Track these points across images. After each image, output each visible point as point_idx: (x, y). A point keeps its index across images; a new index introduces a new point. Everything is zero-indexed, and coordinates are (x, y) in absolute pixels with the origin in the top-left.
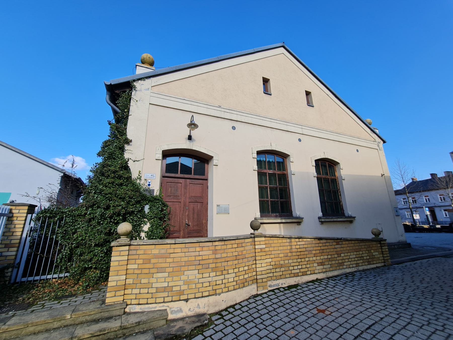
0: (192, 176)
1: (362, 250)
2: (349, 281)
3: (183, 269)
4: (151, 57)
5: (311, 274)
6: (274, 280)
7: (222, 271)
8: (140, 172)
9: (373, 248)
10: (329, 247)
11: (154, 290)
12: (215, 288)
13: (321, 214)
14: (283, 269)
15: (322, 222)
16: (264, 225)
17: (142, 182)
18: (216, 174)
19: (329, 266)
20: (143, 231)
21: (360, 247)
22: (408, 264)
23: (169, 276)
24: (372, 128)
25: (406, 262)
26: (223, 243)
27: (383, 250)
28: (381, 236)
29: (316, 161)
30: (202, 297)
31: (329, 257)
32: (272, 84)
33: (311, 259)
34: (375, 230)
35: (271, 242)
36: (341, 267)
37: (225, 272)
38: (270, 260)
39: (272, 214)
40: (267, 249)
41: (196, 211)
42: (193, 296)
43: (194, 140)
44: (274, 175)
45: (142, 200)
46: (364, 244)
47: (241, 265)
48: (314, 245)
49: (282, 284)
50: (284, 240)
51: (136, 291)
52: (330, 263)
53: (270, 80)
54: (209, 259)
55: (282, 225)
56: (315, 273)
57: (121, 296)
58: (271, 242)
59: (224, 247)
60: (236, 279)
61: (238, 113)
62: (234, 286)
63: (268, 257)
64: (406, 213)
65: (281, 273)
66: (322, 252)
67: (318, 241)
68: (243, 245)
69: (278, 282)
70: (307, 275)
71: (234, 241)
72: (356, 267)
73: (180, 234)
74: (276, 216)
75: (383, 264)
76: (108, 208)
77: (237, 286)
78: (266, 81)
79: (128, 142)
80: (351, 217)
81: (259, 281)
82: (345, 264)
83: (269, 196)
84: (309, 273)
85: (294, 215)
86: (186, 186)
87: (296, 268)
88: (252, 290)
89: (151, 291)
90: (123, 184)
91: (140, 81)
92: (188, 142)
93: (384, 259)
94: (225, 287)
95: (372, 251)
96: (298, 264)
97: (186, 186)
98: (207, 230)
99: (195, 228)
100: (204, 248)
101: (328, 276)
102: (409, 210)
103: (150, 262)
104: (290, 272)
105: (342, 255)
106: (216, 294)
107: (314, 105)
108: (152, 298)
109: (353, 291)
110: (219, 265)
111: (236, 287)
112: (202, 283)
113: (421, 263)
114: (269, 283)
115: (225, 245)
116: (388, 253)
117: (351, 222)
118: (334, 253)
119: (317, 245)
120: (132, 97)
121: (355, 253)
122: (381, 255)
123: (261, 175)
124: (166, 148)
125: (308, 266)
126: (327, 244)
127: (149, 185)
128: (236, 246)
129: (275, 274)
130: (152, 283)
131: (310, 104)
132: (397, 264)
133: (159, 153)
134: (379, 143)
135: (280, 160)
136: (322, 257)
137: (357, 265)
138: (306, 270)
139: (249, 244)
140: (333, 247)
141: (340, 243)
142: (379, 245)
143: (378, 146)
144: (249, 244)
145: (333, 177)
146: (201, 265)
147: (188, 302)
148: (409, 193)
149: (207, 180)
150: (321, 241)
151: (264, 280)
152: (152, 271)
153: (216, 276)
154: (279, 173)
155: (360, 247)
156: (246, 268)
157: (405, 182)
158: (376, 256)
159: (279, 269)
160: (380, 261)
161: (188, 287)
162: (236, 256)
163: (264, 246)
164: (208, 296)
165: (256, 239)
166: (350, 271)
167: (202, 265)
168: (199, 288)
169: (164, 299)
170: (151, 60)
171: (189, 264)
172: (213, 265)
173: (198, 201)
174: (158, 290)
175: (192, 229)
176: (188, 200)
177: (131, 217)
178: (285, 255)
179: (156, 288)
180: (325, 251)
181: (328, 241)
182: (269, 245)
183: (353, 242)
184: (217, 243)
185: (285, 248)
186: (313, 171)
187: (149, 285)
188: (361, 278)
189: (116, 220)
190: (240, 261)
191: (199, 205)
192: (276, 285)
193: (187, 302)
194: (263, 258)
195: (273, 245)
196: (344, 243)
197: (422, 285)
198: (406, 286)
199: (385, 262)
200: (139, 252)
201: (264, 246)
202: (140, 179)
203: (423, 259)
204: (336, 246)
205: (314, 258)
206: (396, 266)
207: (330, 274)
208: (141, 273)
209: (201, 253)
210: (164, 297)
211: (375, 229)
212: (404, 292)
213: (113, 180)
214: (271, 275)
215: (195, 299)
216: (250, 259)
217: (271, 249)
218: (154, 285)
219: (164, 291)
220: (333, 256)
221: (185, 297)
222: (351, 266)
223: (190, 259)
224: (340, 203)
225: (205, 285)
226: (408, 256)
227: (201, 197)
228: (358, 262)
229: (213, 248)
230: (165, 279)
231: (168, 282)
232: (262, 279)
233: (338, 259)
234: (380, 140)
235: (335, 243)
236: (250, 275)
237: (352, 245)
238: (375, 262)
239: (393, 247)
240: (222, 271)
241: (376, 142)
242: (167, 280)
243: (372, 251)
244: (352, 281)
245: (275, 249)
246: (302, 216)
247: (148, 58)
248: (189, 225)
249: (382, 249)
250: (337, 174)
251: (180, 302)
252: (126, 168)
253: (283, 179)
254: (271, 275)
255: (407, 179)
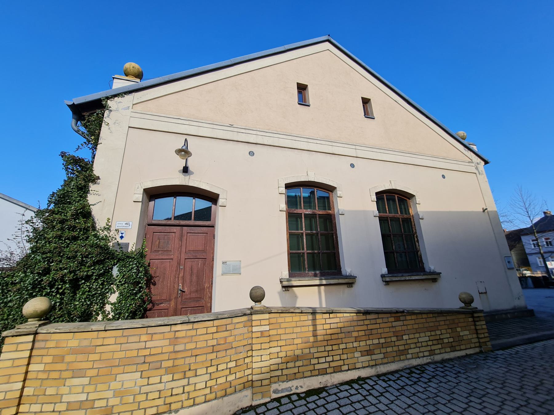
0: (192, 222)
1: (440, 328)
2: (410, 383)
3: (115, 370)
4: (137, 66)
5: (349, 370)
6: (283, 382)
7: (185, 372)
8: (109, 219)
9: (460, 325)
10: (382, 325)
12: (168, 400)
13: (385, 270)
14: (299, 363)
15: (386, 281)
16: (294, 289)
18: (226, 220)
19: (382, 356)
20: (108, 303)
21: (437, 324)
23: (89, 384)
25: (518, 345)
26: (190, 326)
27: (478, 327)
28: (473, 305)
29: (377, 194)
31: (382, 341)
32: (311, 91)
33: (350, 345)
34: (464, 296)
35: (280, 320)
36: (402, 357)
37: (189, 374)
38: (278, 349)
41: (195, 271)
43: (192, 173)
44: (313, 216)
45: (108, 258)
46: (444, 318)
48: (355, 323)
52: (383, 350)
53: (309, 86)
54: (162, 353)
55: (322, 287)
56: (355, 369)
58: (280, 320)
59: (193, 333)
62: (205, 395)
63: (275, 344)
64: (538, 260)
65: (296, 370)
66: (369, 334)
67: (362, 317)
68: (229, 327)
70: (341, 371)
71: (212, 322)
72: (430, 356)
73: (170, 304)
74: (315, 275)
75: (477, 350)
76: (47, 271)
77: (213, 396)
78: (302, 88)
79: (94, 179)
80: (434, 273)
81: (255, 384)
82: (410, 351)
83: (305, 246)
84: (346, 367)
85: (343, 273)
86: (182, 236)
87: (323, 360)
90: (79, 237)
91: (116, 98)
92: (181, 176)
93: (479, 342)
94: (189, 399)
95: (459, 329)
96: (326, 354)
97: (182, 236)
98: (211, 298)
99: (193, 295)
100: (154, 336)
101: (380, 373)
102: (540, 255)
103: (63, 359)
104: (311, 368)
105: (405, 337)
107: (375, 115)
110: (178, 362)
112: (147, 394)
114: (274, 386)
115: (193, 329)
116: (486, 331)
117: (434, 280)
119: (362, 323)
120: (104, 119)
121: (428, 334)
122: (475, 336)
123: (293, 219)
124: (150, 185)
125: (345, 357)
126: (379, 321)
127: (122, 237)
128: (214, 330)
129: (285, 372)
130: (62, 395)
133: (138, 192)
134: (478, 163)
136: (369, 342)
137: (432, 353)
138: (341, 363)
140: (389, 325)
141: (402, 318)
142: (471, 319)
143: (477, 168)
144: (241, 325)
145: (405, 216)
146: (147, 364)
148: (538, 232)
149: (213, 227)
150: (369, 317)
153: (173, 380)
154: (321, 213)
155: (437, 324)
156: (232, 364)
158: (465, 338)
160: (473, 345)
161: (121, 400)
162: (213, 346)
163: (267, 328)
165: (254, 317)
166: (419, 363)
167: (149, 363)
168: (139, 402)
171: (125, 363)
172: (170, 363)
173: (198, 257)
175: (188, 297)
176: (183, 256)
177: (88, 284)
179: (68, 403)
180: (374, 332)
181: (381, 316)
182: (277, 326)
183: (424, 316)
184: (178, 327)
185: (304, 329)
186: (373, 207)
187: (57, 398)
189: (61, 288)
190: (220, 354)
191: (200, 261)
194: (264, 346)
195: (283, 325)
196: (408, 318)
197: (536, 397)
198: (506, 397)
199: (480, 347)
201: (267, 328)
202: (108, 229)
204: (394, 324)
205: (355, 344)
206: (501, 352)
207: (383, 369)
209: (149, 344)
211: (465, 293)
217: (280, 331)
218: (65, 399)
220: (389, 340)
222: (421, 355)
223: (129, 354)
225: (151, 396)
226: (523, 334)
227: (204, 251)
228: (433, 348)
229: (172, 335)
232: (261, 380)
233: (397, 343)
234: (479, 160)
235: (392, 319)
236: (238, 375)
237: (424, 320)
238: (463, 347)
239: (504, 316)
240: (185, 372)
241: (473, 163)
243: (459, 329)
244: (415, 383)
246: (354, 274)
247: (132, 68)
248: (184, 292)
250: (412, 212)
252: (87, 214)
255: (534, 213)
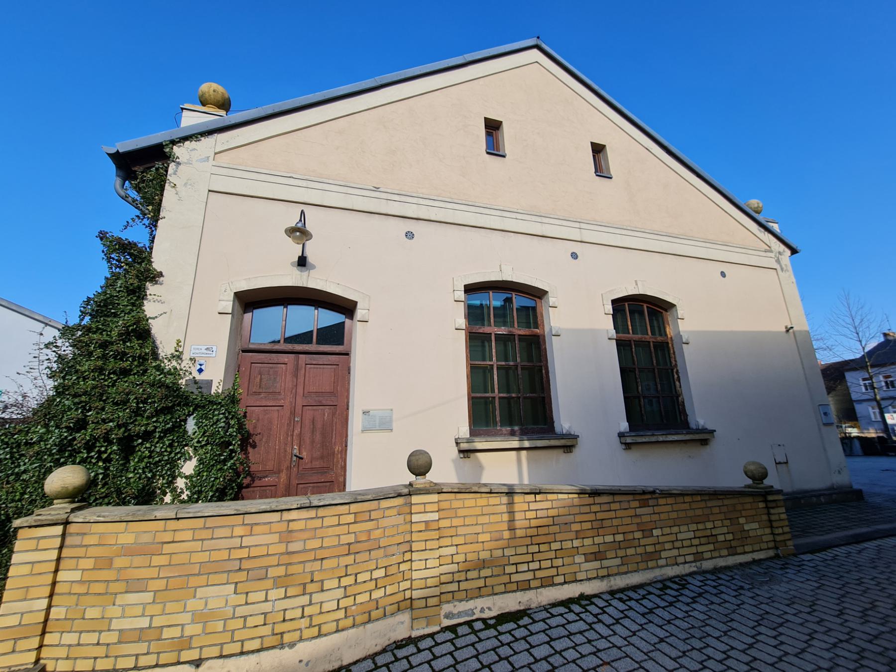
1: (712, 518)
3: (193, 581)
4: (220, 89)
5: (565, 583)
8: (179, 341)
9: (744, 513)
11: (112, 638)
12: (279, 628)
13: (624, 426)
14: (486, 572)
15: (626, 444)
16: (479, 454)
17: (185, 364)
19: (618, 561)
20: (181, 475)
21: (707, 511)
22: (841, 551)
23: (154, 602)
24: (763, 221)
25: (837, 546)
26: (312, 513)
27: (773, 518)
28: (767, 482)
29: (614, 302)
30: (242, 653)
31: (619, 538)
32: (508, 133)
33: (568, 544)
34: (752, 467)
35: (456, 504)
36: (650, 564)
37: (311, 588)
38: (453, 550)
39: (504, 429)
40: (444, 523)
41: (319, 425)
42: (215, 651)
44: (509, 337)
45: (179, 405)
46: (719, 503)
47: (365, 566)
48: (576, 510)
49: (482, 610)
50: (494, 500)
51: (70, 638)
52: (621, 553)
56: (576, 581)
57: (30, 650)
58: (456, 504)
59: (317, 523)
60: (349, 602)
61: (421, 201)
62: (337, 621)
63: (447, 541)
65: (481, 583)
66: (599, 527)
67: (588, 500)
68: (374, 515)
69: (470, 605)
70: (553, 585)
71: (347, 507)
72: (695, 561)
75: (771, 553)
76: (81, 425)
77: (349, 621)
78: (493, 127)
79: (155, 277)
80: (704, 431)
81: (416, 604)
82: (664, 555)
83: (496, 386)
84: (560, 579)
85: (558, 429)
86: (297, 369)
87: (524, 567)
88: (400, 627)
89: (106, 638)
90: (131, 370)
91: (187, 143)
92: (296, 271)
94: (311, 626)
96: (529, 558)
97: (297, 369)
99: (317, 464)
100: (255, 528)
101: (615, 588)
102: (875, 403)
104: (506, 579)
105: (655, 532)
106: (282, 646)
108: (107, 657)
109: (662, 640)
111: (342, 624)
112: (245, 617)
113: (879, 549)
114: (447, 608)
115: (317, 517)
116: (787, 523)
117: (704, 442)
118: (634, 527)
119: (587, 509)
120: (168, 177)
121: (693, 527)
122: (768, 531)
124: (244, 286)
125: (559, 562)
127: (200, 371)
128: (351, 518)
129: (463, 585)
130: (111, 619)
131: (601, 170)
132: (812, 552)
134: (780, 253)
135: (527, 302)
136: (598, 540)
137: (699, 557)
138: (553, 572)
139: (394, 512)
140: (631, 512)
141: (651, 502)
142: (762, 505)
143: (778, 261)
144: (394, 512)
145: (659, 339)
146: (245, 572)
147: (201, 669)
148: (872, 366)
149: (347, 354)
150: (598, 500)
151: (432, 602)
152: (114, 587)
153: (286, 597)
154: (522, 332)
155: (707, 511)
157: (863, 344)
158: (751, 534)
159: (480, 574)
160: (764, 546)
161: (204, 628)
162: (349, 544)
163: (435, 516)
164: (258, 651)
165: (415, 499)
166: (678, 573)
167: (248, 570)
168: (233, 631)
169: (137, 659)
170: (219, 97)
171: (209, 570)
172: (281, 571)
173: (324, 403)
174: (124, 637)
175: (309, 466)
176: (300, 402)
177: (148, 445)
178: (497, 535)
179: (120, 631)
180: (607, 523)
181: (617, 498)
183: (688, 499)
184: (294, 515)
185: (493, 518)
186: (607, 324)
187: (103, 624)
188: (700, 595)
189: (105, 452)
192: (466, 613)
193: (198, 666)
194: (430, 545)
195: (461, 513)
196: (662, 501)
197: (866, 628)
199: (776, 548)
200: (88, 540)
201: (435, 516)
202: (178, 357)
203: (887, 536)
205: (576, 543)
206: (808, 557)
207: (620, 582)
208: (87, 594)
209: (246, 541)
210: (137, 656)
211: (754, 463)
212: (803, 651)
213: (100, 363)
214: (454, 587)
215: (221, 660)
216: (394, 549)
217: (456, 522)
219: (139, 640)
221: (194, 655)
223: (216, 556)
224: (678, 396)
225: (251, 622)
227: (333, 393)
228: (700, 549)
229: (283, 527)
230: (144, 609)
231: (152, 616)
233: (643, 542)
234: (782, 247)
236: (390, 590)
237: (687, 506)
239: (815, 499)
240: (304, 585)
241: (771, 252)
242: (150, 610)
244: (671, 604)
245: (468, 521)
246: (575, 431)
247: (212, 92)
248: (302, 458)
249: (769, 514)
250: (670, 331)
251: (179, 666)
252: (143, 333)
253: (535, 348)
254: (454, 587)
255: (867, 335)
